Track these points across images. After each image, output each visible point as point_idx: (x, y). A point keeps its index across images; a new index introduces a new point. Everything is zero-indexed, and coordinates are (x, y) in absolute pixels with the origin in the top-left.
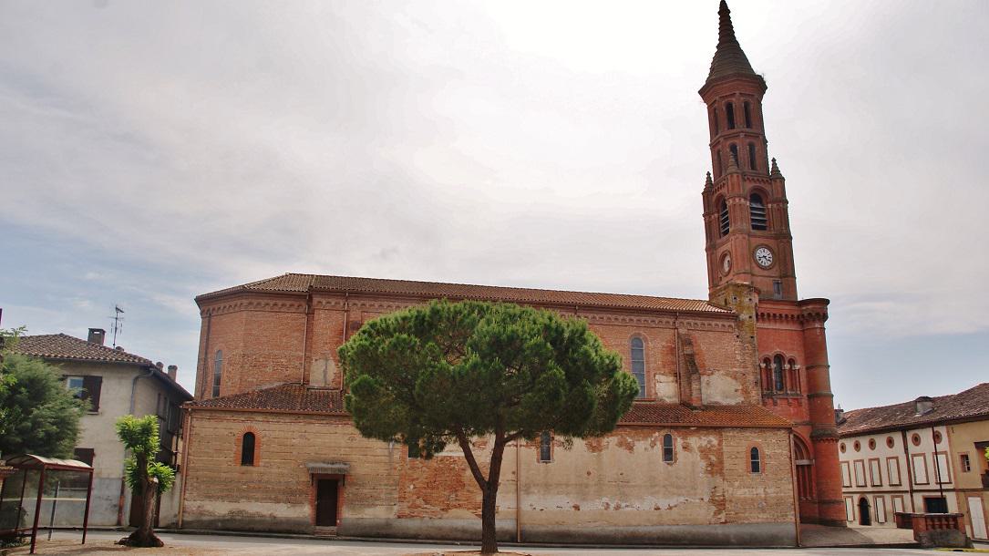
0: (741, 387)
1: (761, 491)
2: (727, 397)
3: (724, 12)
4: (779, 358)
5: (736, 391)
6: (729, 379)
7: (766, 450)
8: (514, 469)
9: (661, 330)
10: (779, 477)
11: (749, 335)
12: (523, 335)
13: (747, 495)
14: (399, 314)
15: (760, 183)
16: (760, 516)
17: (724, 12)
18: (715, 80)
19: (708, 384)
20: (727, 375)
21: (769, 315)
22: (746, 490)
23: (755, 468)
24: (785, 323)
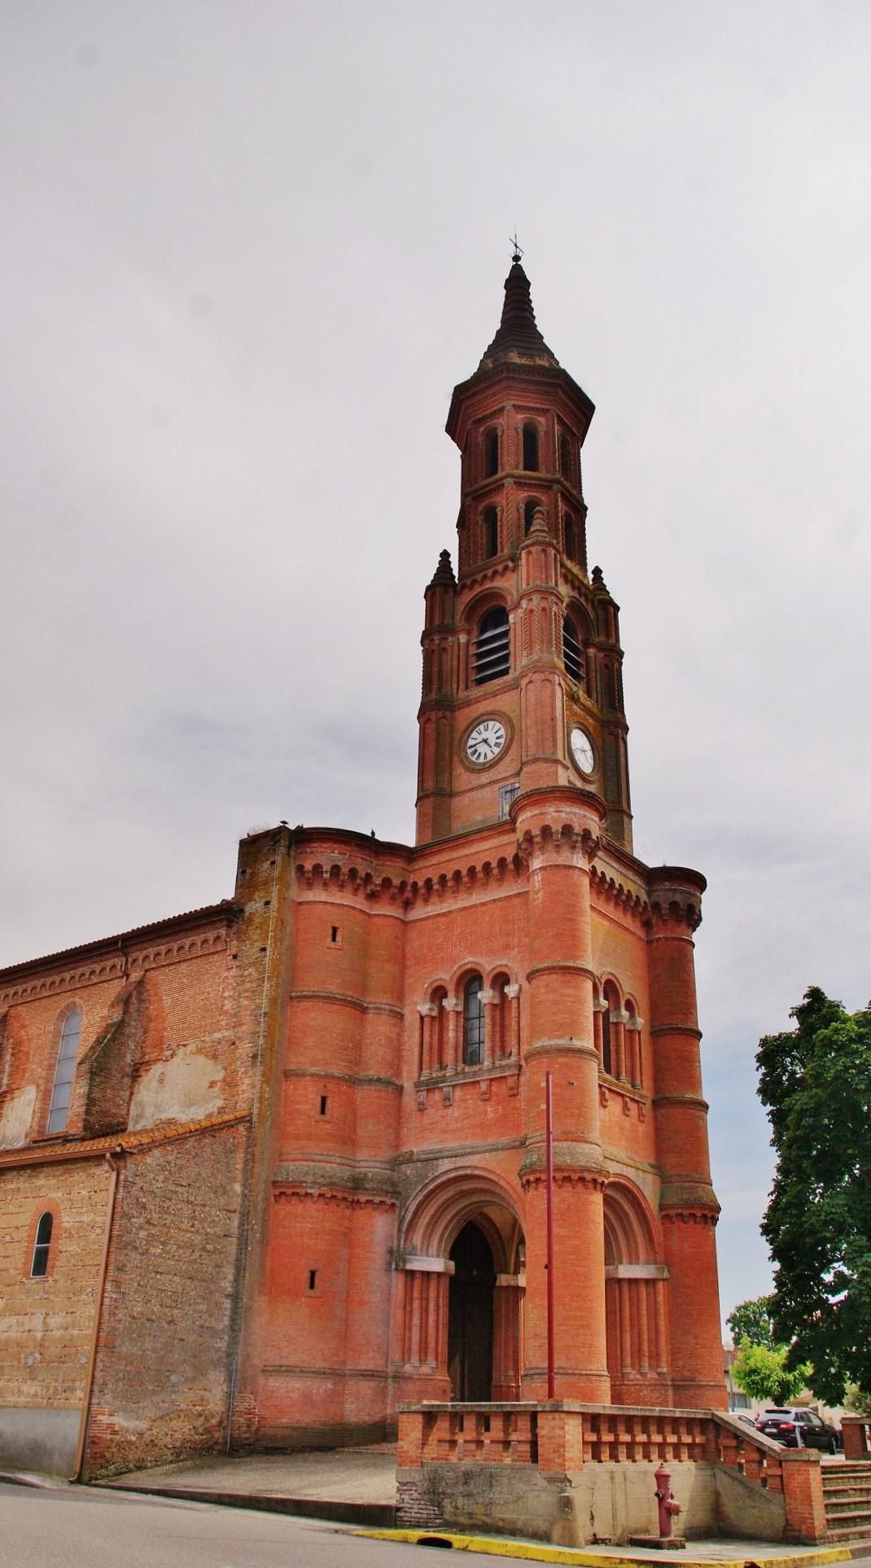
0: (220, 1076)
1: (37, 1322)
2: (190, 1105)
3: (517, 285)
4: (470, 981)
5: (212, 1084)
6: (202, 1059)
7: (65, 1220)
8: (545, 1261)
9: (106, 985)
10: (78, 1285)
11: (259, 945)
12: (369, 1059)
13: (13, 1334)
14: (8, 1057)
15: (586, 600)
16: (25, 1388)
17: (517, 285)
18: (465, 447)
19: (161, 1081)
20: (199, 1051)
21: (443, 878)
22: (13, 1320)
23: (41, 1264)
24: (334, 889)
